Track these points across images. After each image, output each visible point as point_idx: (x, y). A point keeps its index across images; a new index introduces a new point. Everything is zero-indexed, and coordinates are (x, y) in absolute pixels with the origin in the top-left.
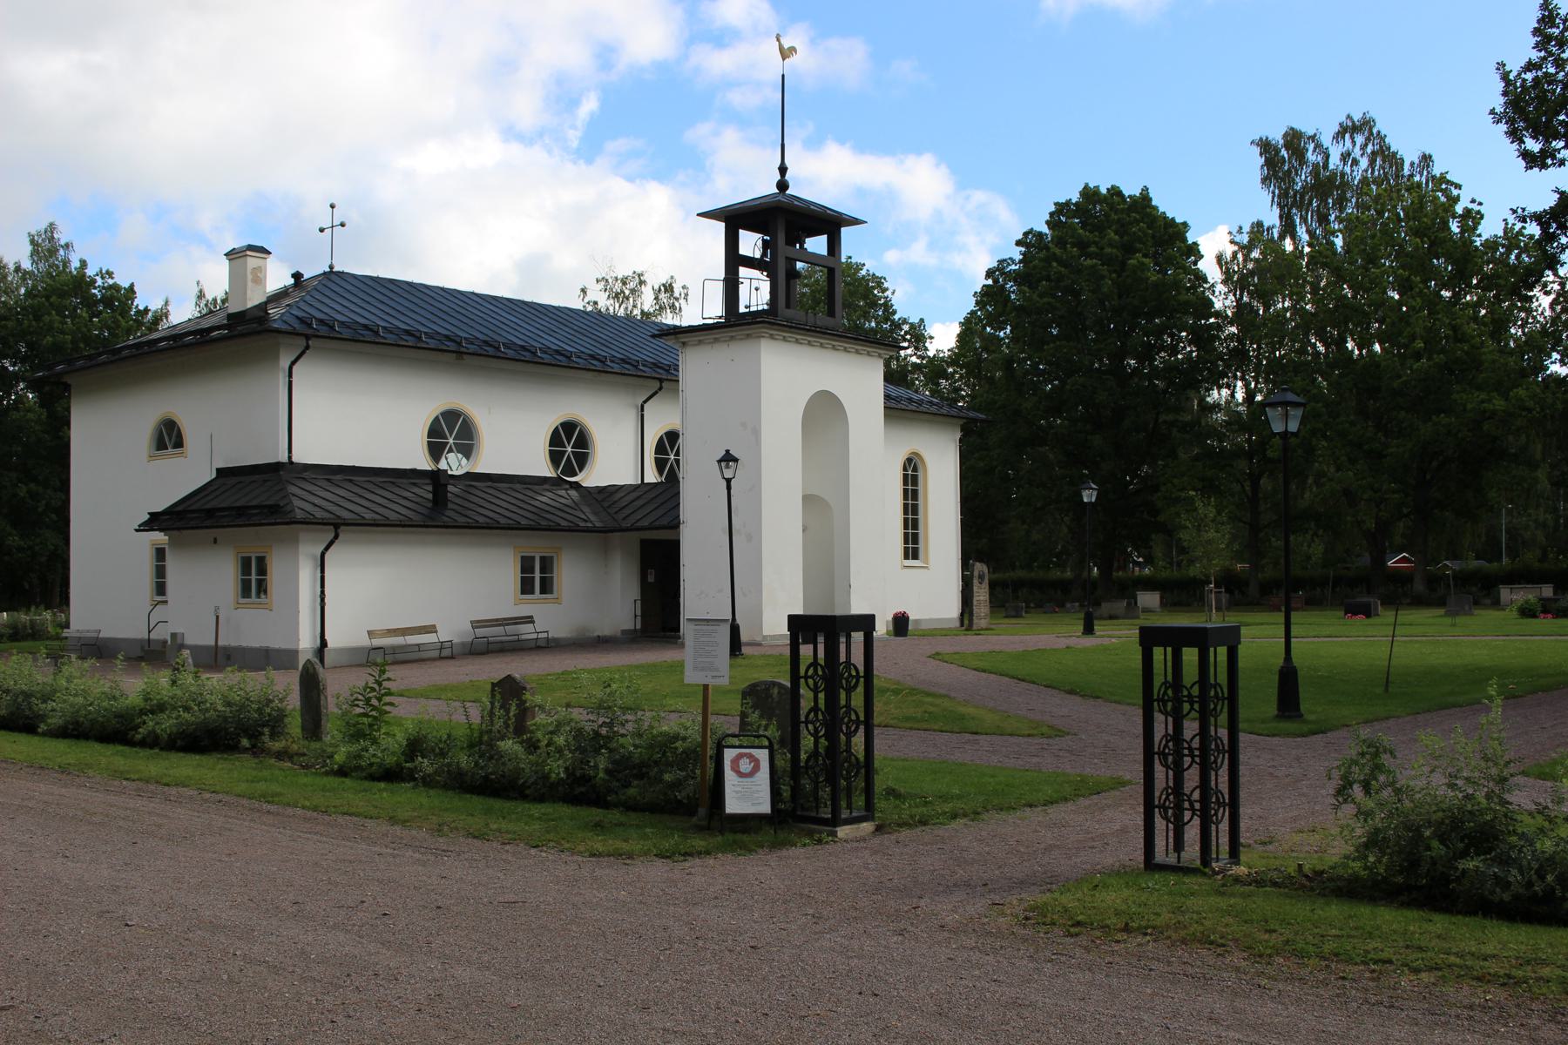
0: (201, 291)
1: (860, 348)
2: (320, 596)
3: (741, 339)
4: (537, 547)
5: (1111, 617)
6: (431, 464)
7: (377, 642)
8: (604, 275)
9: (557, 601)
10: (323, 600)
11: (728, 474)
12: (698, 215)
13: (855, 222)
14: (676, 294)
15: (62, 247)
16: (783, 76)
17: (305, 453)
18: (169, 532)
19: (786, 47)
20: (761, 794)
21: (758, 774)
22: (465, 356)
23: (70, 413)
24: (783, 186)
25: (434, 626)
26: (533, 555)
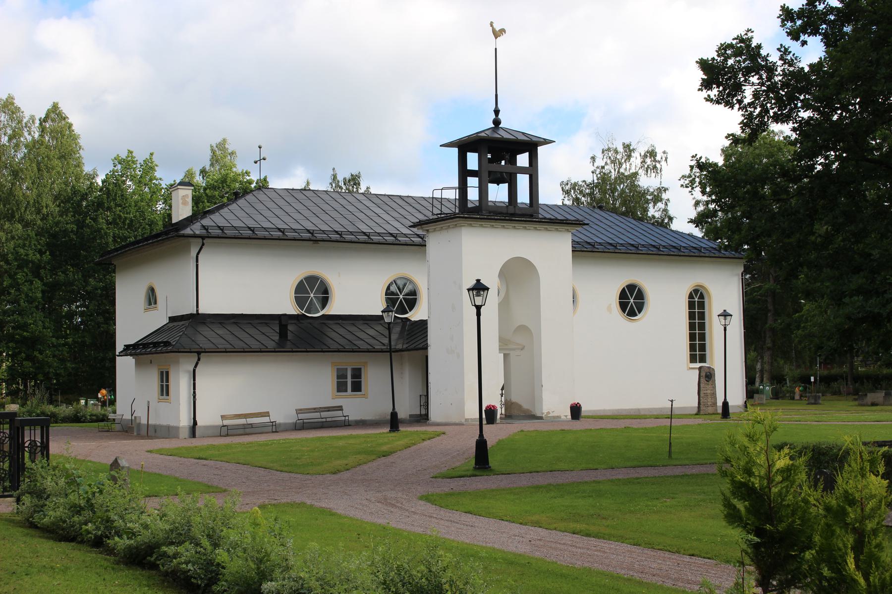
1: (537, 226)
4: (350, 362)
5: (874, 404)
7: (226, 422)
9: (365, 396)
10: (194, 397)
11: (479, 300)
12: (441, 146)
13: (546, 142)
16: (496, 49)
17: (207, 307)
18: (135, 356)
19: (497, 30)
22: (319, 242)
24: (497, 122)
25: (268, 413)
26: (345, 367)
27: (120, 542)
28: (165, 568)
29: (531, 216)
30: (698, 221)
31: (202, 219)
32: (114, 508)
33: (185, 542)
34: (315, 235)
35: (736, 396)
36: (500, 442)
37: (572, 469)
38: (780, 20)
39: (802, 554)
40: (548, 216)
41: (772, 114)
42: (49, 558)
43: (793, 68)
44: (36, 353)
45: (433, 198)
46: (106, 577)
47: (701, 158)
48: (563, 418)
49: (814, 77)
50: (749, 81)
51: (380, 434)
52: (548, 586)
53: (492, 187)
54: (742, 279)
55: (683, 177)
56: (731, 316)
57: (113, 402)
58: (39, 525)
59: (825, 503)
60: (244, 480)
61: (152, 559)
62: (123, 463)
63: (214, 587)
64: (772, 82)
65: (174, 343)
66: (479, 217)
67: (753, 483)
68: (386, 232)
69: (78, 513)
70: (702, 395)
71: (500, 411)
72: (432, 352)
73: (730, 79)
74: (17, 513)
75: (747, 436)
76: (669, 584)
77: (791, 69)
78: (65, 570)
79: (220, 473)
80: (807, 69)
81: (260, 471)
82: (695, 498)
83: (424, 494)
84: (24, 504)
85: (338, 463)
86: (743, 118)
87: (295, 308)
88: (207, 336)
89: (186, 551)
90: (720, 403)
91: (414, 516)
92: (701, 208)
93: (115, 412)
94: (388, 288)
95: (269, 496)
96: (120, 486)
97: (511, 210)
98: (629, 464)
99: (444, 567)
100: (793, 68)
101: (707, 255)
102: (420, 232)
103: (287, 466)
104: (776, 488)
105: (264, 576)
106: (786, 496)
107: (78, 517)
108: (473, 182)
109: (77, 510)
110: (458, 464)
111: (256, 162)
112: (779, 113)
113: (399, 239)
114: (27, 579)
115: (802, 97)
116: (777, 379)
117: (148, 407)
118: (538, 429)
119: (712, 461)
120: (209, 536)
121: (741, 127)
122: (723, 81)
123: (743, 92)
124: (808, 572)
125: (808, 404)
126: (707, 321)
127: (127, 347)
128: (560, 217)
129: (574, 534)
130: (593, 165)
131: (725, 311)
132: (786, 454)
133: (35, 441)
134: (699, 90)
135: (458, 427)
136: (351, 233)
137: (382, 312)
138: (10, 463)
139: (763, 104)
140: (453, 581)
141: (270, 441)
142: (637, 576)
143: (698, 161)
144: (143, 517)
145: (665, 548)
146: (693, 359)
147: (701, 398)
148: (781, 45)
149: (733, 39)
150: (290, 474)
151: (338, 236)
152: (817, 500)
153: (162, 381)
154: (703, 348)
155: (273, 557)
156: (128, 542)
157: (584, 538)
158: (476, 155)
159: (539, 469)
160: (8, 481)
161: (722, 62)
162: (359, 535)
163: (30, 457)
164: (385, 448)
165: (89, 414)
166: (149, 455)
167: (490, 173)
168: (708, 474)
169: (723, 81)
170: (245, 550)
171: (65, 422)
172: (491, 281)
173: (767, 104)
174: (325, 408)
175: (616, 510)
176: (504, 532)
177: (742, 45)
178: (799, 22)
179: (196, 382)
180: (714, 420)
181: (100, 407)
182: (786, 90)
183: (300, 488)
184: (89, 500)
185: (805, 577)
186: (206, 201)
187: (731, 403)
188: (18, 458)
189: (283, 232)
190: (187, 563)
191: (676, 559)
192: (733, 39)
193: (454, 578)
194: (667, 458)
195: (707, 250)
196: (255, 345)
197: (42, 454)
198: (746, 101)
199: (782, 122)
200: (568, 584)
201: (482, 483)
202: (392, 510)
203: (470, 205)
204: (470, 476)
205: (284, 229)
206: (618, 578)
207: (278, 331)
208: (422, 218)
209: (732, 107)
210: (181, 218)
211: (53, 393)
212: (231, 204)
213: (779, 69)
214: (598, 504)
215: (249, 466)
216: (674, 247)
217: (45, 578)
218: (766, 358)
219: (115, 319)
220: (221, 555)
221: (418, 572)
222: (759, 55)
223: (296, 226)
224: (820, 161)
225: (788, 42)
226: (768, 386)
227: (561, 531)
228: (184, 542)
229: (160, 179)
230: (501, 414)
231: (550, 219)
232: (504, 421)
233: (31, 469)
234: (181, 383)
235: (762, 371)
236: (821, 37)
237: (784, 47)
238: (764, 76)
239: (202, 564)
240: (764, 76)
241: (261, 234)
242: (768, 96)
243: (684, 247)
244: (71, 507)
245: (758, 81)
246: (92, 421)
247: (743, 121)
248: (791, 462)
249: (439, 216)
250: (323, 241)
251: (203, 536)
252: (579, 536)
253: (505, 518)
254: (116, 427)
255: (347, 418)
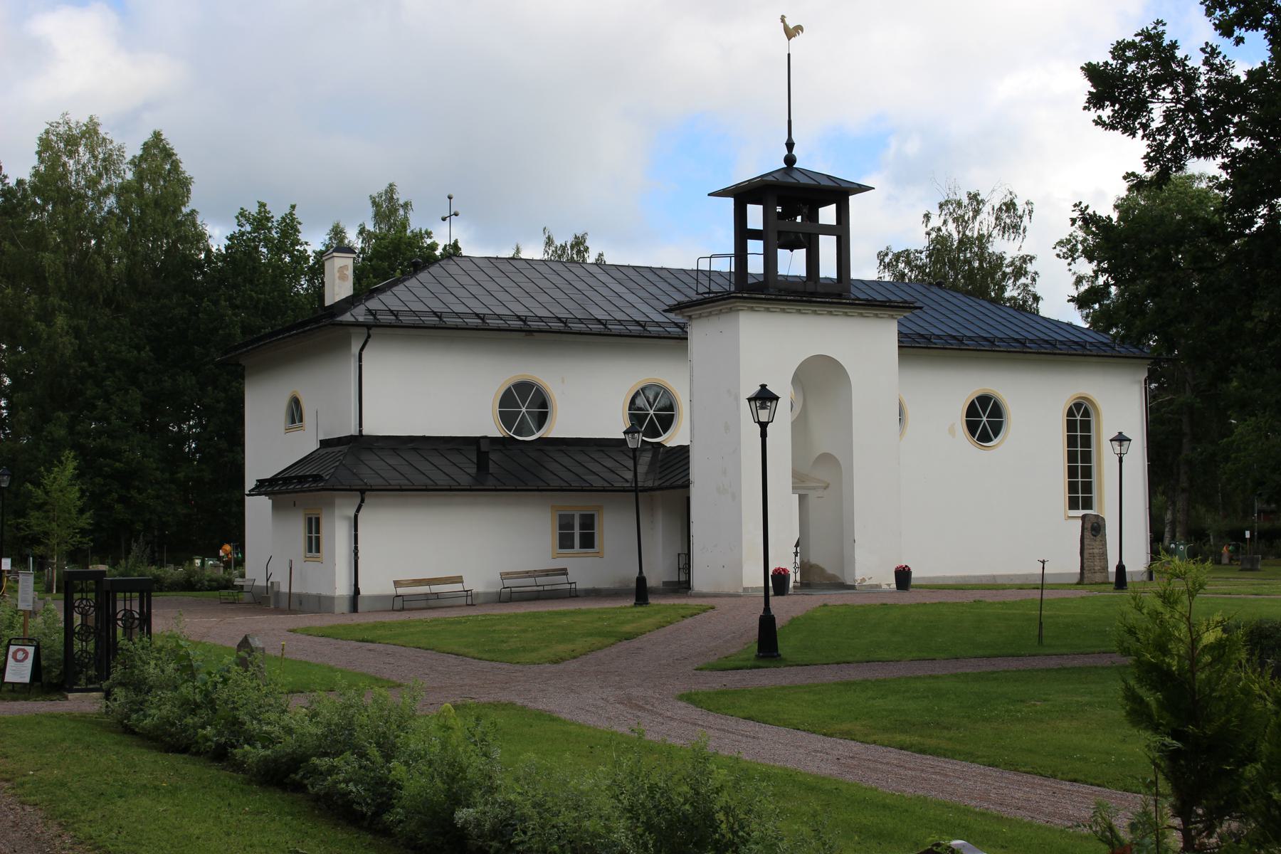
0: (549, 238)
2: (354, 551)
3: (727, 312)
4: (577, 505)
6: (502, 432)
7: (401, 591)
8: (946, 198)
11: (764, 415)
12: (709, 195)
13: (862, 189)
14: (1020, 212)
15: (402, 206)
16: (789, 55)
19: (791, 27)
20: (26, 672)
21: (27, 660)
22: (535, 334)
23: (244, 395)
24: (790, 160)
27: (251, 752)
28: (316, 789)
29: (840, 296)
30: (1082, 301)
31: (367, 300)
32: (243, 705)
33: (346, 751)
34: (529, 323)
35: (1137, 558)
36: (793, 621)
37: (898, 659)
38: (1204, 7)
39: (1241, 770)
40: (862, 296)
41: (1191, 144)
42: (151, 774)
43: (1224, 77)
44: (134, 493)
45: (698, 270)
46: (231, 801)
47: (1087, 207)
48: (884, 587)
49: (1253, 90)
50: (1159, 95)
51: (621, 608)
52: (865, 821)
53: (782, 254)
54: (1146, 388)
55: (1061, 243)
56: (1130, 440)
57: (240, 563)
58: (137, 730)
59: (1275, 692)
60: (427, 671)
61: (298, 777)
62: (256, 642)
63: (385, 817)
64: (1192, 98)
65: (327, 478)
66: (763, 296)
67: (1169, 665)
68: (630, 319)
69: (193, 712)
70: (1086, 556)
71: (794, 578)
72: (696, 493)
73: (1130, 92)
74: (107, 713)
75: (1160, 596)
76: (1040, 820)
77: (1222, 77)
78: (174, 791)
79: (393, 661)
80: (1243, 78)
81: (449, 659)
82: (1078, 701)
83: (685, 692)
84: (115, 700)
85: (562, 648)
86: (1149, 150)
87: (498, 423)
88: (375, 467)
89: (346, 764)
90: (1112, 568)
91: (672, 723)
92: (1085, 286)
93: (243, 576)
94: (633, 401)
95: (463, 694)
96: (253, 674)
97: (810, 287)
98: (980, 652)
99: (717, 788)
100: (1224, 77)
101: (1094, 353)
102: (679, 319)
103: (489, 651)
104: (1202, 673)
105: (457, 800)
106: (1217, 684)
107: (192, 718)
108: (755, 246)
109: (193, 708)
110: (733, 651)
111: (444, 219)
112: (1202, 142)
113: (649, 329)
114: (120, 802)
115: (1236, 120)
116: (1196, 536)
117: (291, 568)
118: (848, 603)
119: (1102, 649)
120: (378, 745)
121: (1145, 163)
122: (1120, 95)
123: (1150, 112)
124: (1250, 795)
125: (1241, 570)
126: (1094, 449)
127: (261, 483)
128: (880, 298)
129: (902, 748)
130: (926, 226)
131: (1120, 433)
132: (1218, 622)
133: (131, 611)
134: (1085, 108)
135: (734, 599)
136: (581, 321)
137: (625, 433)
138: (96, 643)
139: (1178, 129)
140: (730, 808)
141: (463, 617)
142: (995, 810)
143: (1082, 212)
144: (286, 717)
145: (1035, 771)
146: (1073, 504)
147: (1085, 561)
148: (1207, 43)
149: (1136, 35)
150: (493, 663)
151: (562, 325)
152: (1264, 689)
153: (310, 532)
154: (1088, 488)
155: (470, 773)
156: (262, 752)
157: (917, 755)
158: (760, 208)
159: (850, 659)
160: (93, 668)
161: (1119, 69)
162: (591, 747)
163: (124, 634)
164: (628, 628)
165: (208, 579)
166: (292, 635)
167: (780, 233)
168: (1096, 667)
169: (1120, 95)
170: (430, 763)
171: (172, 591)
172: (782, 387)
173: (1183, 129)
174: (542, 571)
175: (963, 717)
176: (800, 746)
177: (1149, 43)
178: (1232, 10)
179: (359, 545)
180: (1104, 591)
181: (222, 569)
182: (1212, 109)
183: (506, 683)
184: (207, 694)
185: (1247, 802)
186: (371, 276)
187: (1129, 568)
188: (108, 633)
189: (483, 319)
190: (347, 782)
191: (1051, 787)
192: (1136, 35)
193: (732, 804)
194: (1036, 644)
195: (1095, 346)
196: (442, 480)
197: (142, 629)
198: (1155, 125)
199: (1206, 156)
200: (894, 818)
201: (768, 678)
202: (639, 714)
203: (750, 281)
204: (751, 668)
205: (484, 315)
206: (967, 811)
207: (475, 461)
208: (680, 298)
209: (1133, 134)
210: (337, 299)
211: (156, 549)
212: (408, 279)
213: (1203, 78)
214: (936, 708)
215: (434, 652)
216: (1047, 342)
217: (146, 801)
218: (1180, 504)
219: (244, 444)
220: (397, 769)
221: (679, 794)
222: (1173, 57)
223: (500, 310)
224: (1262, 213)
225: (1214, 38)
226: (1182, 544)
227: (883, 745)
228: (342, 752)
229: (306, 243)
230: (795, 581)
231: (867, 300)
232: (799, 592)
233: (127, 650)
234: (337, 533)
235: (1173, 523)
236: (1264, 32)
237: (1211, 46)
238: (1180, 89)
239: (368, 784)
240: (1180, 89)
241: (450, 321)
242: (1186, 118)
243: (1061, 341)
244: (183, 705)
245: (1171, 97)
246: (211, 589)
247: (1148, 153)
248: (1225, 636)
249: (707, 295)
250: (540, 331)
251: (370, 743)
252: (909, 753)
253: (801, 727)
254: (245, 597)
255: (573, 586)
